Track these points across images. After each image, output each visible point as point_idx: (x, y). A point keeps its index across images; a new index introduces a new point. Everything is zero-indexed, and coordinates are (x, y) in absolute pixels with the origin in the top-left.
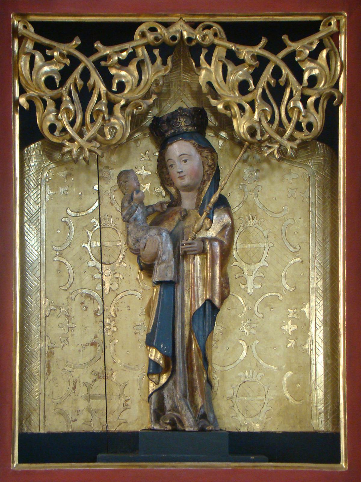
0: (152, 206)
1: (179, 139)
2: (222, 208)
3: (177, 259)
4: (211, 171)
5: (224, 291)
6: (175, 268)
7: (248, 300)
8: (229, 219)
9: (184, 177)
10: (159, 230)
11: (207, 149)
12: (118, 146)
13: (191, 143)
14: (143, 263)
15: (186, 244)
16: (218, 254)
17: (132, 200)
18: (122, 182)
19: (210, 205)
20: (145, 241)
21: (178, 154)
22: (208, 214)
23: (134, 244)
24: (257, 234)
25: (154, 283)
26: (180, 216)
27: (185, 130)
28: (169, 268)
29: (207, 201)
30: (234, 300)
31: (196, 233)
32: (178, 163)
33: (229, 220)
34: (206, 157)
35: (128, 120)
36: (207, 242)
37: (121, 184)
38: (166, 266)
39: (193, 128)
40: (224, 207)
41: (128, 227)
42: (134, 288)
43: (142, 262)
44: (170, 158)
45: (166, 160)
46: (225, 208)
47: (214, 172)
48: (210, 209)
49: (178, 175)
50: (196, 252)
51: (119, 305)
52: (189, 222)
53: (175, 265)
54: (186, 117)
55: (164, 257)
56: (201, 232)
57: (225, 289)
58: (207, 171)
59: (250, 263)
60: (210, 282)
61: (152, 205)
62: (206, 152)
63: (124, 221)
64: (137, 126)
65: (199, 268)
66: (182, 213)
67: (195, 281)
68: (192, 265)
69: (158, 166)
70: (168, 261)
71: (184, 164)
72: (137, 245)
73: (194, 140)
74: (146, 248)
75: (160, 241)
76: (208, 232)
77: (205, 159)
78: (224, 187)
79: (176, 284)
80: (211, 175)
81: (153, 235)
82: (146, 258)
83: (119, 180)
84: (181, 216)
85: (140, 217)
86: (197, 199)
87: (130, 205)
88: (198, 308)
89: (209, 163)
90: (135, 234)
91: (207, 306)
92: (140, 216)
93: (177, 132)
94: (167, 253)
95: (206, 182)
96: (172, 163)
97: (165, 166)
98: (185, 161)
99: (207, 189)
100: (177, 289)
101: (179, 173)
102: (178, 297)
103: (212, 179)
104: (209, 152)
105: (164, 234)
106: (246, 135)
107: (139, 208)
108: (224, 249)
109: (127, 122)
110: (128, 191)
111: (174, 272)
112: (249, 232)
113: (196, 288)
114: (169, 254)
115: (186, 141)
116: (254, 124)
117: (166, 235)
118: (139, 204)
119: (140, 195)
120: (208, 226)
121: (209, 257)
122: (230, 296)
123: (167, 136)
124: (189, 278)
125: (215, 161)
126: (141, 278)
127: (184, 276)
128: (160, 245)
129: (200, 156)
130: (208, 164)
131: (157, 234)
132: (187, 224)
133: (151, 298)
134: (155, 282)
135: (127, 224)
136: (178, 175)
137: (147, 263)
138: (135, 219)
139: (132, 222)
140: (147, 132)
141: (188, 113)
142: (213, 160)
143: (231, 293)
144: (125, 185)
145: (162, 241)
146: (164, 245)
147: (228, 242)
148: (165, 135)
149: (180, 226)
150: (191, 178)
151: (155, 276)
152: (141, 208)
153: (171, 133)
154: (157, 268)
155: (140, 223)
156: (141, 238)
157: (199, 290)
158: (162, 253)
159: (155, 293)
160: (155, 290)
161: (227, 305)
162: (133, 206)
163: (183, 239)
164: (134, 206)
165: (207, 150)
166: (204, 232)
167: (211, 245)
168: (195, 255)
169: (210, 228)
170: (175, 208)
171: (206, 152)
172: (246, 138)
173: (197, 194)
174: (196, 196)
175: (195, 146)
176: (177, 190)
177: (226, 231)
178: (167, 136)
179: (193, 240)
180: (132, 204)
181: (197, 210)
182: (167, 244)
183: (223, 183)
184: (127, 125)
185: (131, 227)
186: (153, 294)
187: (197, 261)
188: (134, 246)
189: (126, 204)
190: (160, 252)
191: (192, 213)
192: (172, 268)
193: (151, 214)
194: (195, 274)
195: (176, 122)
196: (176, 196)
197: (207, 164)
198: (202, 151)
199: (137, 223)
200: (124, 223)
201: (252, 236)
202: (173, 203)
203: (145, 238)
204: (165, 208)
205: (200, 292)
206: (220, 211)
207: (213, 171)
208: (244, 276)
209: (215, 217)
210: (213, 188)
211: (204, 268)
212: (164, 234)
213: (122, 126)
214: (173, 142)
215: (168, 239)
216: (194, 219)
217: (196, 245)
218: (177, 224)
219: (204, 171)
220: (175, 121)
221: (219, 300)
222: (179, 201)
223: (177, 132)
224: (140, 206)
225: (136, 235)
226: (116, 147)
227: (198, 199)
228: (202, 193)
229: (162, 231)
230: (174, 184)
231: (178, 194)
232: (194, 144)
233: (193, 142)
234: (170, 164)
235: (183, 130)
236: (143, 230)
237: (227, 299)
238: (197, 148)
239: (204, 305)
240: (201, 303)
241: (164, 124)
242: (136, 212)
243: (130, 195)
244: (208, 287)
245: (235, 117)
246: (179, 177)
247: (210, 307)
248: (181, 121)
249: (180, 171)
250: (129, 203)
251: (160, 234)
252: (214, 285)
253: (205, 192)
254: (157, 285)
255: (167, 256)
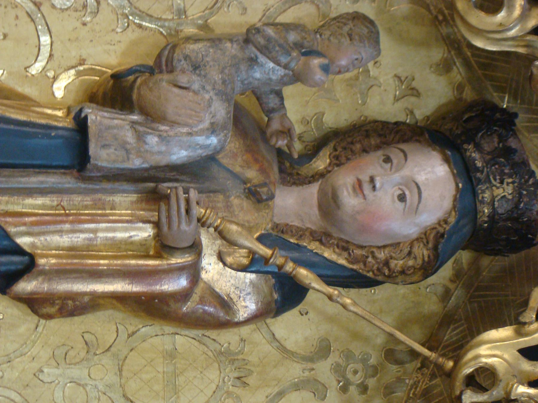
0: (282, 106)
1: (458, 180)
2: (276, 296)
3: (146, 174)
4: (375, 267)
5: (53, 304)
6: (123, 169)
7: (23, 370)
8: (246, 315)
9: (361, 196)
10: (224, 127)
11: (432, 257)
12: (432, 14)
13: (450, 214)
14: (135, 81)
15: (188, 201)
16: (158, 287)
17: (305, 54)
18: (349, 26)
19: (289, 267)
20: (196, 86)
21: (421, 178)
22: (266, 260)
23: (186, 57)
24: (202, 391)
25: (81, 110)
26: (256, 181)
27: (483, 197)
28: (123, 153)
29: (296, 255)
30: (22, 329)
31: (216, 229)
32: (397, 177)
33: (242, 315)
34: (410, 253)
35: (516, 43)
36: (190, 259)
37: (345, 24)
38: (128, 147)
39: (486, 219)
40: (276, 301)
41: (231, 41)
42: (56, 54)
43: (137, 78)
44: (408, 156)
45: (403, 146)
46: (273, 305)
47: (370, 275)
48: (280, 267)
49: (365, 178)
50: (165, 229)
51: (9, 8)
52: (242, 208)
53: (131, 170)
54: (516, 199)
55: (152, 140)
56: (215, 239)
57: (57, 307)
58: (374, 257)
59: (124, 374)
60: (80, 267)
61: (284, 107)
62: (426, 253)
63: (248, 30)
64: (484, 66)
65: (120, 235)
66: (265, 189)
67: (86, 226)
68: (128, 215)
69: (385, 124)
70: (142, 149)
71: (393, 195)
72: (185, 66)
73: (458, 222)
74: (176, 90)
75: (195, 129)
76: (214, 259)
77: (406, 250)
78: (338, 302)
79: (79, 171)
80: (362, 267)
81: (212, 109)
82: (151, 90)
83: (354, 18)
84: (255, 186)
85: (258, 75)
86: (298, 229)
87: (293, 49)
88: (11, 234)
89: (396, 262)
90: (214, 60)
91: (16, 259)
92: (261, 73)
93: (478, 175)
94: (163, 148)
95: (345, 254)
96: (395, 161)
97: (384, 143)
98: (402, 198)
99: (326, 255)
100: (64, 174)
101: (372, 180)
102: (41, 178)
103: (352, 270)
104: (423, 260)
105: (214, 140)
106: (473, 363)
107: (281, 72)
108: (168, 305)
109: (511, 43)
110: (327, 42)
111: (111, 169)
112: (207, 366)
113: (67, 226)
114: (160, 153)
115: (455, 200)
116: (502, 385)
117: (212, 146)
118: (292, 71)
119: (319, 76)
120: (229, 260)
121: (151, 262)
122: (36, 318)
123: (466, 150)
124: (94, 206)
125: (400, 278)
126: (92, 71)
127: (99, 196)
128: (185, 130)
129: (415, 236)
130: (391, 258)
131: (212, 121)
132: (236, 202)
133: (35, 102)
134: (83, 115)
135: (241, 38)
136: (365, 178)
137: (136, 91)
138: (253, 61)
139: (247, 51)
140: (469, 95)
141: (525, 204)
142: (403, 272)
143: (43, 321)
144: (341, 34)
145: (197, 134)
146: (185, 139)
147: (185, 315)
148: (469, 144)
149: (229, 183)
150: (358, 212)
151: (101, 113)
152: (282, 77)
153: (475, 160)
154: (121, 119)
155: (244, 75)
156: (205, 76)
157: (61, 236)
158: (165, 134)
159: (49, 111)
160: (60, 113)
161: (9, 311)
162: (290, 55)
163: (200, 192)
164: (289, 58)
165: (429, 257)
166: (216, 248)
167: (181, 269)
168: (157, 225)
169: (225, 264)
170: (276, 169)
171: (426, 253)
172: (466, 363)
173: (313, 228)
174: (309, 226)
175: (439, 223)
176: (321, 175)
177: (215, 307)
178: (466, 150)
179: (199, 220)
180: (294, 54)
181: (273, 229)
182: (188, 147)
183: (348, 301)
184: (504, 43)
185: (231, 49)
186: (49, 108)
187: (140, 229)
188: (181, 57)
189: (292, 37)
190: (167, 128)
191: (263, 216)
192: (123, 161)
193: (261, 104)
194: (104, 225)
195: (502, 174)
196: (306, 170)
197: (394, 255)
198: (428, 243)
199: (243, 67)
200: (245, 31)
201: (195, 377)
202: (287, 164)
203: (203, 88)
204: (277, 141)
205: (56, 240)
206: (266, 289)
207: (373, 272)
208: (89, 357)
209: (253, 276)
210: (329, 273)
211: (119, 249)
212: (214, 140)
213: (503, 28)
214: (452, 166)
215: (200, 151)
216: (248, 222)
217: (184, 227)
218: (235, 176)
219: (374, 247)
220: (506, 171)
221: (33, 293)
222: (292, 180)
223: (478, 175)
224: (285, 75)
225: (211, 63)
226: (429, 11)
227: (300, 233)
228: (317, 243)
229: (222, 134)
230: (338, 165)
231: (313, 176)
232: (446, 222)
233: (452, 220)
234: (392, 156)
235: (483, 192)
236: (224, 82)
237: (29, 311)
238: (434, 228)
239: (19, 251)
240: (24, 241)
241: (496, 140)
242: (271, 65)
243: (315, 48)
244: (69, 261)
245: (519, 334)
246: (360, 183)
247: (13, 268)
248: (505, 185)
249: (378, 185)
250: (298, 46)
251: (213, 129)
252: (76, 278)
253: (319, 252)
254: (74, 118)
255: (156, 149)
